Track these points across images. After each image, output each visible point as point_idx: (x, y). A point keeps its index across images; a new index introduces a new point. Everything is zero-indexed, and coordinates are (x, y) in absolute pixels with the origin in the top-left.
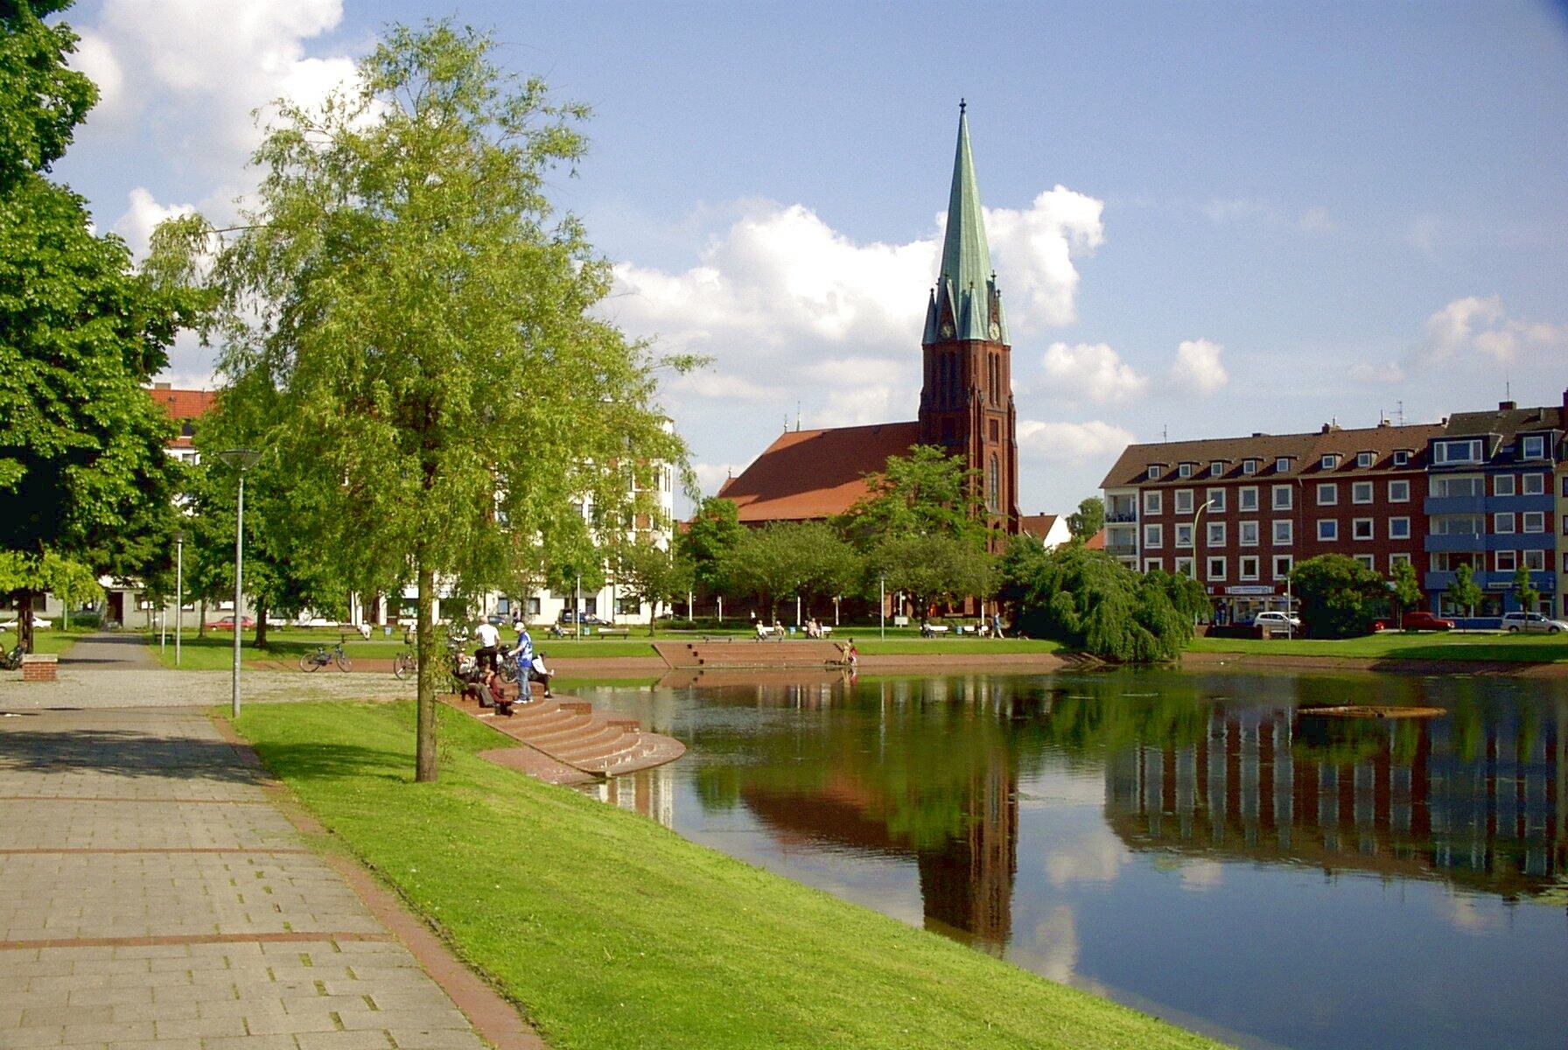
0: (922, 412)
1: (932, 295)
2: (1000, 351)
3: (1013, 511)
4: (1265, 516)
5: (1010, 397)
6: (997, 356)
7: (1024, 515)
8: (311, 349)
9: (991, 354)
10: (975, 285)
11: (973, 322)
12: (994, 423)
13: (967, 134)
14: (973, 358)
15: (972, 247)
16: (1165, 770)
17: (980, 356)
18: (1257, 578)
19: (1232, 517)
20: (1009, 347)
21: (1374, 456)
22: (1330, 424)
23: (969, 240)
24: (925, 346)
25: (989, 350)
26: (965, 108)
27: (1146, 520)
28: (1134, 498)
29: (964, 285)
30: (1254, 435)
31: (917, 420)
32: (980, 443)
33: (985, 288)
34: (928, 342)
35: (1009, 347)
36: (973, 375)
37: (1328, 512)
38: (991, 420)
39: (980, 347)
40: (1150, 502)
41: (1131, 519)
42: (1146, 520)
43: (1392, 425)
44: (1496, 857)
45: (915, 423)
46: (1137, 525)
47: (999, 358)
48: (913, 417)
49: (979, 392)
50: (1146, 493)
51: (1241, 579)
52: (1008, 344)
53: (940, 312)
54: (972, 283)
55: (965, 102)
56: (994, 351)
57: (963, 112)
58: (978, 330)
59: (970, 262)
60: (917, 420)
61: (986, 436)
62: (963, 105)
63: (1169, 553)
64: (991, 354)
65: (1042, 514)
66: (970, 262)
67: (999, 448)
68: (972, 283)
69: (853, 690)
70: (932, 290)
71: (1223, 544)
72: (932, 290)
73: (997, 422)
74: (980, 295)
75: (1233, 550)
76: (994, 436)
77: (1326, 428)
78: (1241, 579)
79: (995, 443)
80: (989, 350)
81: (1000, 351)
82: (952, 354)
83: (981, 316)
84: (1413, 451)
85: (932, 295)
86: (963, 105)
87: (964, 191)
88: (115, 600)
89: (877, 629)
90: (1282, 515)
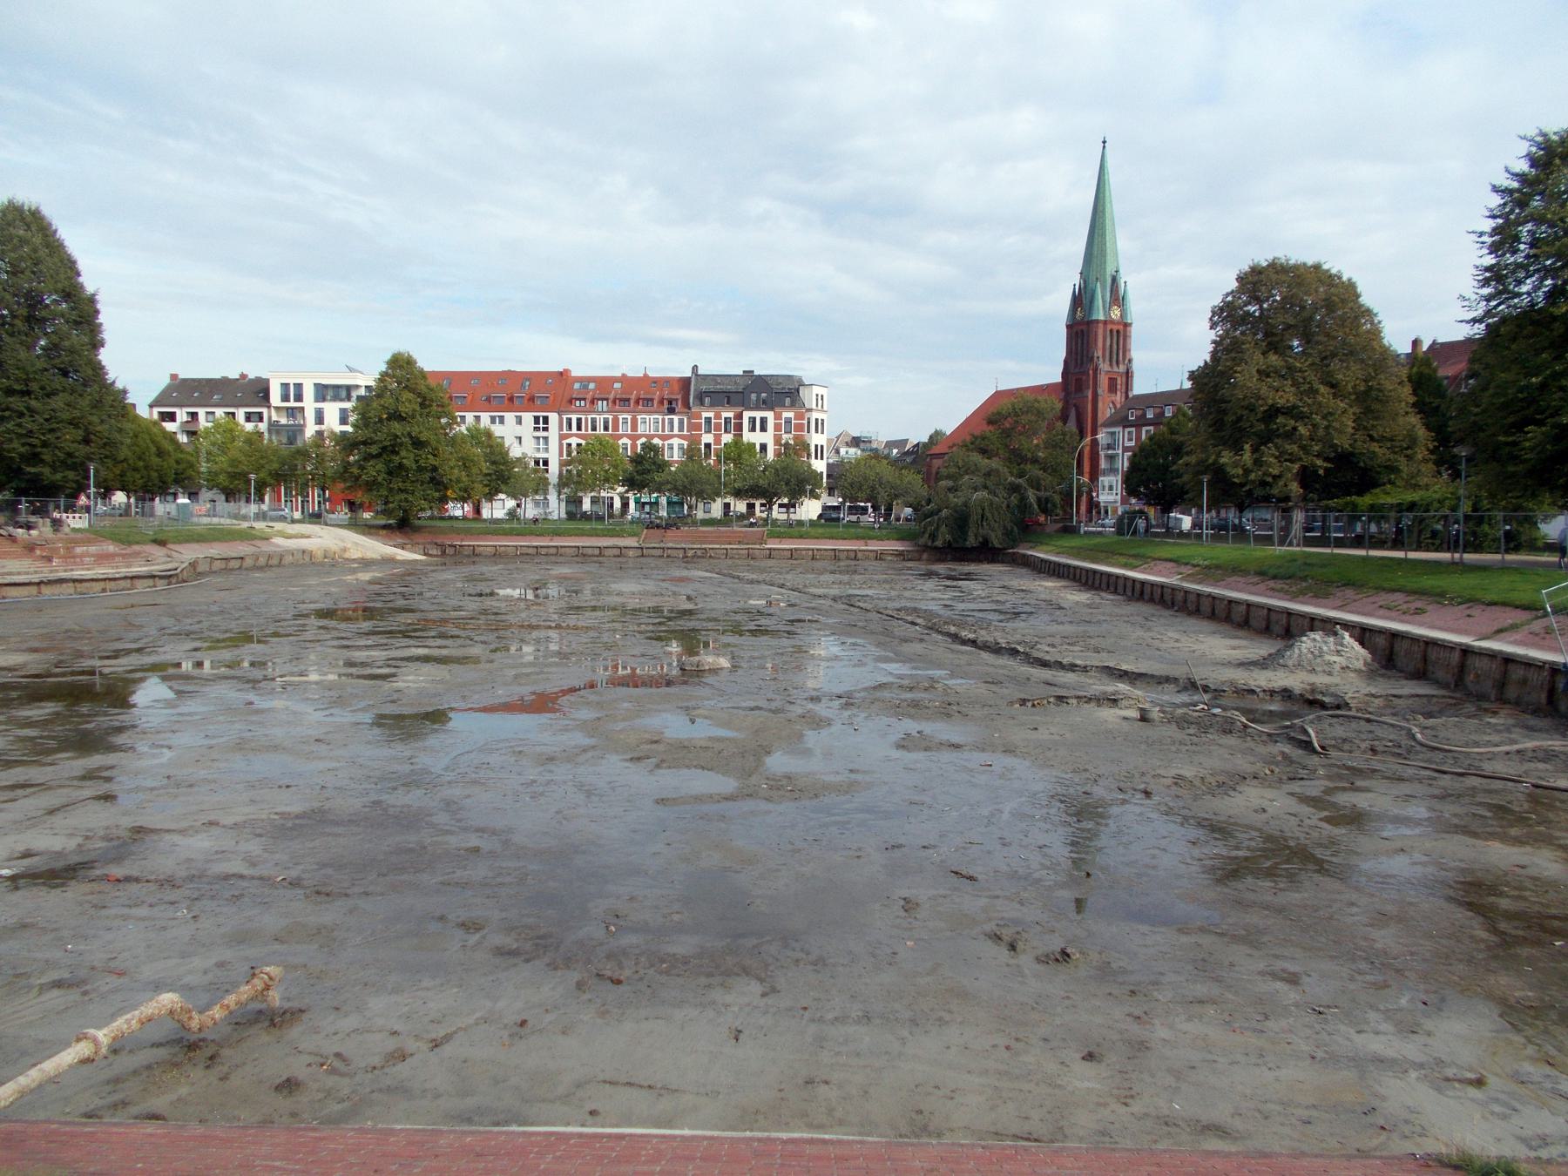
0: (1065, 374)
2: (1121, 327)
5: (1130, 361)
24: (1067, 326)
25: (1109, 327)
38: (1110, 379)
39: (1101, 325)
47: (1120, 333)
50: (1127, 430)
53: (1081, 300)
56: (1115, 328)
57: (1104, 147)
62: (1104, 142)
64: (1077, 333)
81: (1121, 328)
82: (1082, 331)
83: (1104, 302)
86: (1104, 142)
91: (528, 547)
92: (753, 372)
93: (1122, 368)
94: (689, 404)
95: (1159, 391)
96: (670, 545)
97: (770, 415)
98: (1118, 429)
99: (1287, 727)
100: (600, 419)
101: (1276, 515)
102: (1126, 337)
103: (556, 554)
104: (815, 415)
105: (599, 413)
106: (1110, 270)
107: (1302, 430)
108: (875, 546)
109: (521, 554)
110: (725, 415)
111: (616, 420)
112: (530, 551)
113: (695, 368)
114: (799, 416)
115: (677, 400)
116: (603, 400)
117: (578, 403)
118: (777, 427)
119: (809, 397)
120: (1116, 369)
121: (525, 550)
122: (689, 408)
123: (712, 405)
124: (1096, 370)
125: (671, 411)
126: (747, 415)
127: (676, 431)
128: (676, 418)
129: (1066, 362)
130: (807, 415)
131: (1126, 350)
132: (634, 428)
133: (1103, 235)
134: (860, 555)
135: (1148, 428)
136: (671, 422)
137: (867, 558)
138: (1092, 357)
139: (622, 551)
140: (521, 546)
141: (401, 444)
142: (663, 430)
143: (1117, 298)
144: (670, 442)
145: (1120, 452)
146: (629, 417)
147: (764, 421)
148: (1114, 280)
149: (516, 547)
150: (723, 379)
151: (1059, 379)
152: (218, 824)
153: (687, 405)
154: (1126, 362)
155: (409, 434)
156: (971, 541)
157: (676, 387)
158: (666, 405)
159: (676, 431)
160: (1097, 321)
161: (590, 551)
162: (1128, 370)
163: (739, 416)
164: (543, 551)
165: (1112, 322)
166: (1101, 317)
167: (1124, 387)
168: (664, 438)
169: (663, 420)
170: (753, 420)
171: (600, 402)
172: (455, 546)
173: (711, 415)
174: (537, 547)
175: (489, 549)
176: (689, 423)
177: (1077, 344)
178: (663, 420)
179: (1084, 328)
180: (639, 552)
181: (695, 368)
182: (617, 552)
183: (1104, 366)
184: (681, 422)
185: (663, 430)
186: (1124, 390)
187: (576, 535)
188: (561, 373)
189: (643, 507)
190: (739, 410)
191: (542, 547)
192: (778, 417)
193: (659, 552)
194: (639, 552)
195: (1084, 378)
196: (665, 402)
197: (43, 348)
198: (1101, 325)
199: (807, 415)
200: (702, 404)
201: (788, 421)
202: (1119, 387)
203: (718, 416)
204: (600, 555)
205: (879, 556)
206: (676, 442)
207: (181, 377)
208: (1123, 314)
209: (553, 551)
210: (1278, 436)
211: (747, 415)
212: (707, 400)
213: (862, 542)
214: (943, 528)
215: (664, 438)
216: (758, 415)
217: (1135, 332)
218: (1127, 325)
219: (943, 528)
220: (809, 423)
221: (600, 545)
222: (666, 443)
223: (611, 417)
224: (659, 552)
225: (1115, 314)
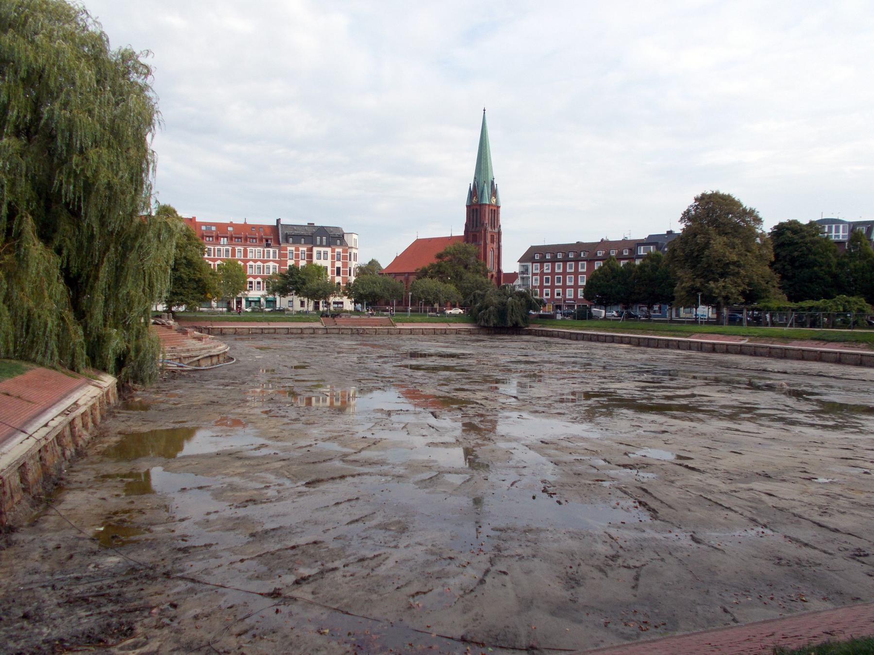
0: (466, 232)
2: (496, 208)
3: (499, 271)
4: (576, 273)
8: (67, 641)
12: (492, 236)
24: (467, 206)
32: (485, 244)
33: (490, 184)
39: (487, 207)
42: (534, 274)
44: (101, 322)
45: (458, 238)
47: (495, 211)
50: (534, 264)
53: (475, 193)
56: (493, 208)
67: (495, 246)
74: (488, 187)
76: (492, 241)
81: (496, 208)
82: (477, 209)
88: (104, 177)
90: (582, 273)
91: (256, 328)
92: (194, 218)
93: (496, 230)
94: (279, 241)
95: (547, 244)
96: (343, 327)
97: (329, 250)
98: (530, 264)
100: (223, 249)
101: (710, 310)
102: (498, 213)
103: (275, 333)
104: (354, 251)
105: (224, 245)
106: (490, 179)
107: (742, 272)
108: (454, 326)
109: (252, 333)
110: (301, 249)
111: (234, 251)
112: (258, 331)
113: (278, 221)
114: (345, 251)
115: (271, 239)
116: (224, 237)
117: (207, 239)
118: (333, 257)
119: (349, 240)
121: (254, 331)
122: (280, 244)
123: (294, 243)
124: (485, 230)
125: (268, 246)
126: (315, 249)
127: (271, 258)
128: (271, 250)
129: (466, 225)
130: (349, 250)
131: (498, 220)
132: (245, 254)
133: (486, 159)
134: (448, 332)
135: (583, 262)
136: (269, 252)
137: (451, 333)
138: (483, 224)
139: (314, 330)
140: (252, 328)
141: (180, 264)
142: (264, 257)
143: (494, 193)
144: (267, 264)
145: (530, 276)
146: (242, 249)
147: (326, 253)
148: (493, 183)
149: (249, 328)
150: (298, 228)
151: (462, 234)
152: (667, 432)
153: (278, 242)
155: (185, 258)
156: (509, 324)
157: (268, 231)
158: (264, 242)
159: (271, 258)
160: (486, 204)
161: (295, 331)
163: (311, 250)
164: (266, 331)
165: (492, 205)
166: (488, 203)
168: (264, 262)
169: (264, 251)
170: (319, 253)
171: (222, 239)
172: (209, 329)
173: (293, 249)
174: (262, 329)
175: (231, 330)
176: (279, 253)
177: (473, 216)
178: (264, 251)
179: (478, 208)
180: (325, 331)
181: (278, 221)
182: (311, 331)
183: (489, 229)
184: (274, 253)
185: (264, 257)
187: (289, 321)
188: (191, 220)
189: (250, 304)
190: (310, 246)
191: (265, 329)
192: (333, 251)
193: (337, 331)
194: (325, 331)
196: (264, 240)
198: (487, 207)
199: (349, 250)
200: (287, 241)
201: (339, 254)
203: (297, 250)
204: (314, 333)
205: (458, 332)
206: (271, 264)
208: (497, 201)
209: (272, 331)
210: (730, 275)
211: (315, 249)
212: (291, 240)
213: (446, 324)
214: (492, 317)
215: (264, 262)
216: (322, 249)
217: (501, 210)
218: (498, 207)
219: (492, 317)
220: (350, 255)
221: (301, 327)
222: (265, 265)
223: (230, 248)
224: (337, 331)
225: (494, 201)
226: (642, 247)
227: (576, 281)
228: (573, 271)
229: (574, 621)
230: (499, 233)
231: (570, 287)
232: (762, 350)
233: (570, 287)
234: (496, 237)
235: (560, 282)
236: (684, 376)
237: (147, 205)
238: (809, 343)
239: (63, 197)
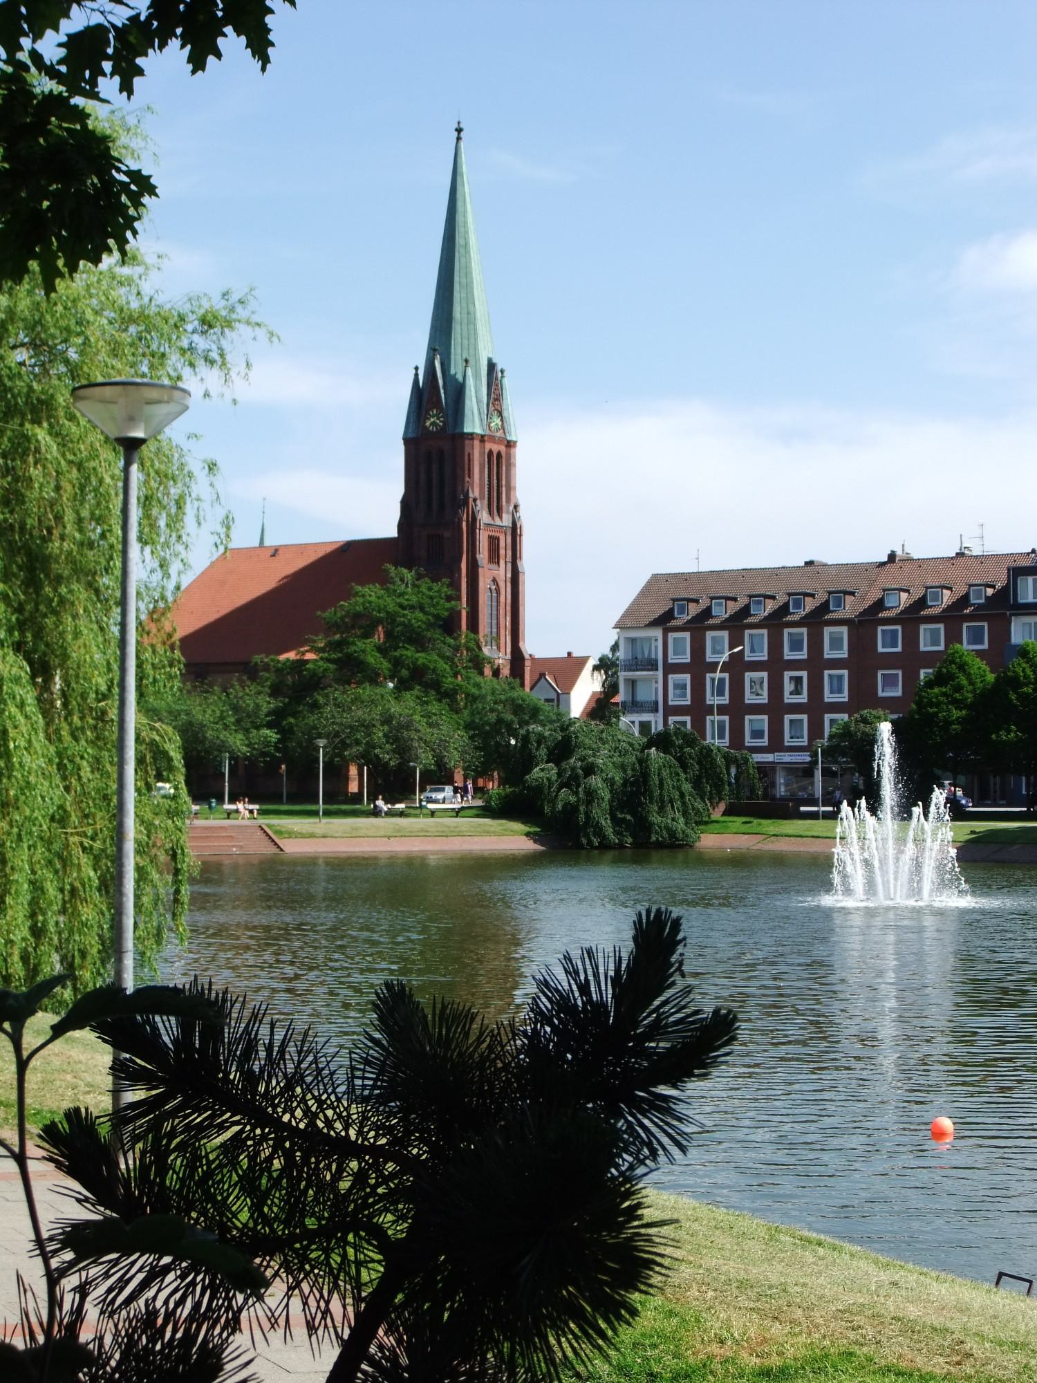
0: (401, 526)
1: (416, 375)
2: (503, 449)
3: (517, 658)
5: (516, 507)
6: (499, 454)
7: (539, 655)
9: (491, 452)
10: (471, 362)
11: (467, 411)
12: (494, 541)
13: (465, 168)
14: (466, 457)
15: (468, 313)
16: (901, 1020)
17: (477, 454)
18: (765, 742)
19: (775, 665)
20: (515, 443)
21: (946, 592)
22: (899, 552)
23: (464, 305)
24: (407, 441)
25: (488, 446)
26: (462, 134)
27: (670, 669)
28: (656, 640)
29: (456, 369)
30: (807, 563)
31: (395, 535)
34: (410, 435)
35: (515, 443)
36: (467, 479)
37: (889, 661)
38: (490, 537)
39: (477, 443)
40: (680, 647)
41: (652, 665)
42: (670, 669)
43: (974, 554)
46: (660, 673)
48: (392, 532)
49: (475, 500)
50: (671, 636)
51: (786, 744)
52: (514, 439)
54: (466, 361)
55: (462, 126)
56: (496, 448)
57: (459, 139)
58: (473, 421)
59: (465, 333)
60: (395, 535)
61: (483, 556)
62: (459, 130)
63: (699, 709)
64: (491, 452)
65: (569, 654)
66: (465, 333)
67: (502, 572)
68: (466, 361)
69: (828, 913)
70: (417, 368)
71: (803, 698)
72: (417, 368)
73: (498, 539)
74: (477, 376)
75: (776, 708)
76: (494, 557)
77: (892, 557)
78: (786, 744)
79: (494, 566)
80: (488, 446)
81: (503, 449)
82: (441, 452)
83: (478, 402)
84: (993, 587)
85: (416, 375)
86: (459, 130)
87: (459, 241)
89: (313, 807)
90: (835, 664)
93: (506, 521)
99: (65, 705)
102: (510, 465)
120: (498, 522)
154: (511, 508)
160: (471, 436)
162: (514, 523)
165: (492, 439)
166: (478, 430)
167: (509, 553)
183: (484, 517)
186: (509, 558)
195: (447, 534)
197: (501, 1126)
198: (477, 443)
202: (502, 552)
207: (574, 655)
217: (521, 457)
218: (510, 445)
219: (51, 626)
226: (1030, 579)
227: (776, 688)
228: (803, 655)
229: (136, 770)
230: (515, 531)
231: (756, 709)
232: (442, 814)
233: (756, 709)
234: (505, 542)
235: (840, 691)
236: (758, 959)
237: (511, 978)
238: (797, 855)
239: (662, 998)
